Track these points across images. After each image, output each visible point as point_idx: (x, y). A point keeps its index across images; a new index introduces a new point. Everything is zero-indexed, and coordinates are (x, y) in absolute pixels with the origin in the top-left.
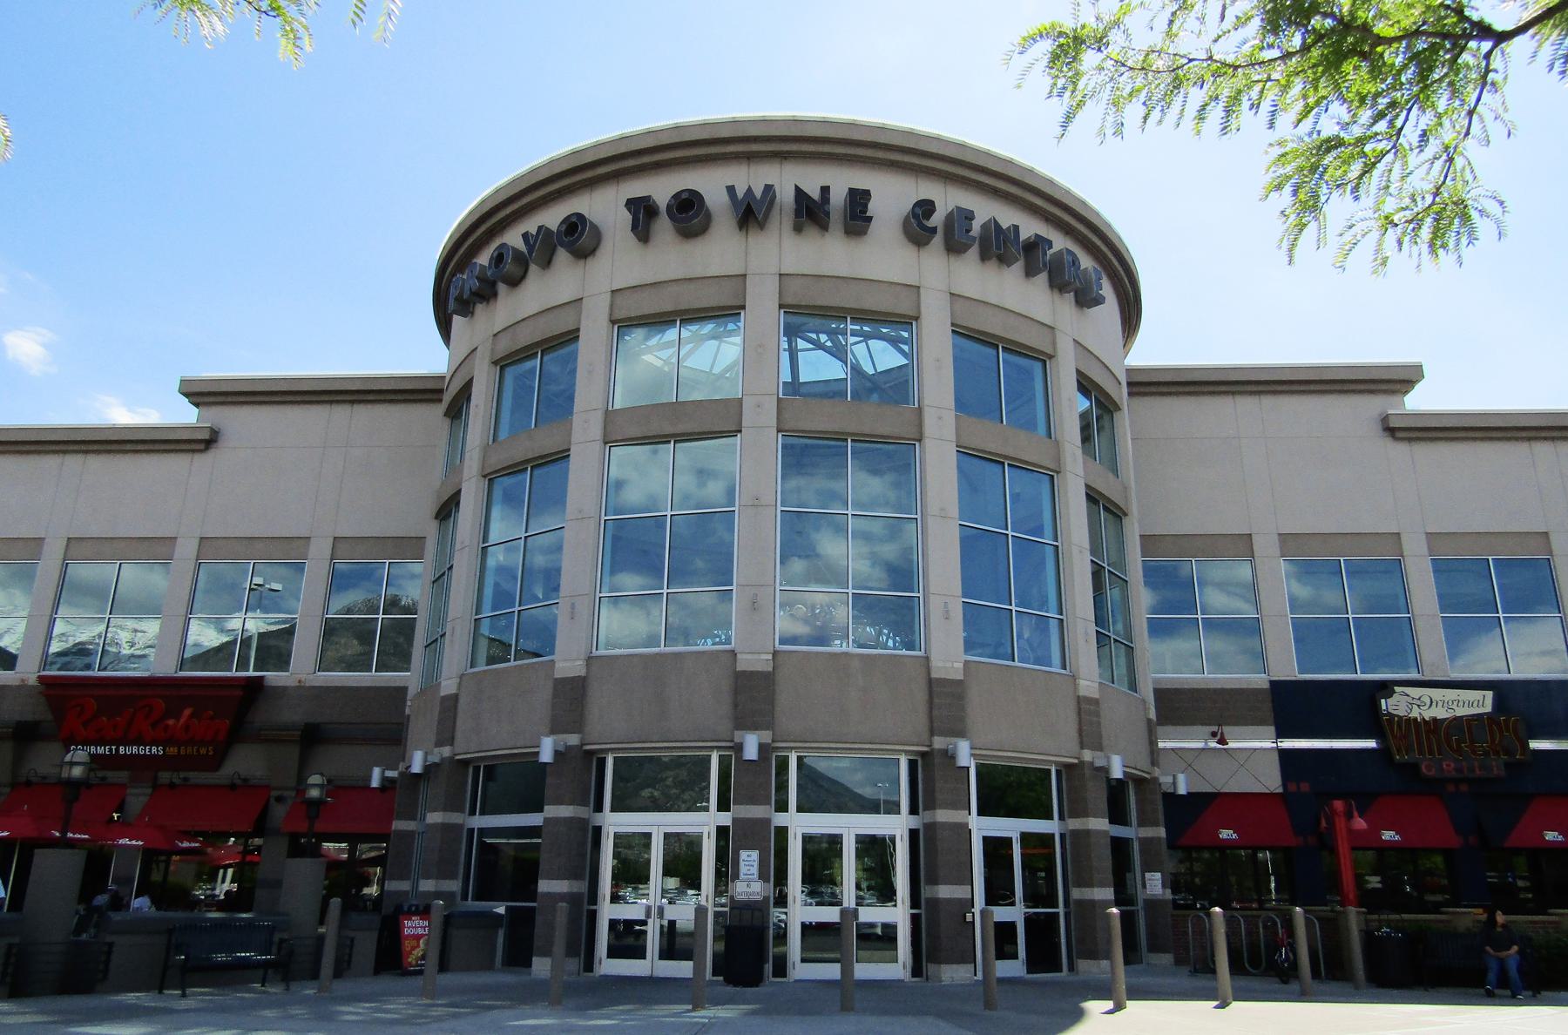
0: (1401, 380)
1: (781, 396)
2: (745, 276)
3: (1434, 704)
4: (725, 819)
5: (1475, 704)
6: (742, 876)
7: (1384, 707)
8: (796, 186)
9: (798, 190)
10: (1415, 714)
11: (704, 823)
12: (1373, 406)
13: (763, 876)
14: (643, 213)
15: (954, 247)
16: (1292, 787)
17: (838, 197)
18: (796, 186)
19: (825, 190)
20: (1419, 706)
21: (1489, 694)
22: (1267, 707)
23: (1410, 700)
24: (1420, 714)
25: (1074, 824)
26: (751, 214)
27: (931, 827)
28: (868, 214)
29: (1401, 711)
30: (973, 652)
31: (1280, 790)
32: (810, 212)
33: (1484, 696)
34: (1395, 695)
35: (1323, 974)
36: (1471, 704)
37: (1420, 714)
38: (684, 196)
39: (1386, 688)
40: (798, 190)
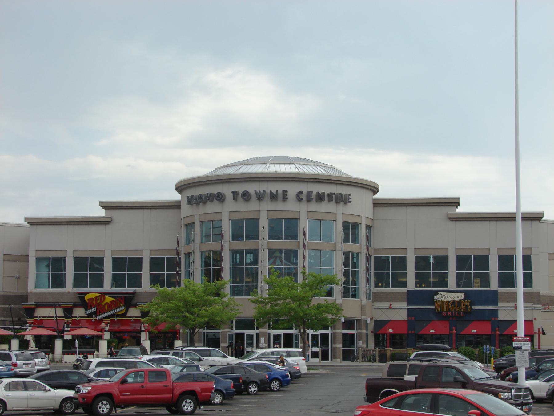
0: (456, 203)
1: (268, 240)
2: (259, 211)
3: (448, 297)
4: (258, 331)
5: (459, 297)
6: (261, 343)
7: (435, 298)
8: (270, 191)
9: (271, 192)
10: (443, 300)
11: (254, 332)
12: (449, 211)
13: (265, 342)
14: (235, 194)
15: (309, 200)
16: (410, 318)
17: (280, 192)
18: (270, 191)
19: (277, 191)
20: (444, 297)
21: (463, 294)
22: (406, 297)
23: (442, 296)
24: (444, 299)
25: (359, 331)
26: (260, 197)
27: (335, 333)
28: (287, 197)
29: (439, 299)
30: (152, 363)
31: (407, 319)
32: (274, 197)
33: (462, 295)
34: (438, 295)
35: (524, 393)
36: (458, 297)
37: (444, 299)
38: (245, 192)
39: (436, 293)
40: (271, 192)
